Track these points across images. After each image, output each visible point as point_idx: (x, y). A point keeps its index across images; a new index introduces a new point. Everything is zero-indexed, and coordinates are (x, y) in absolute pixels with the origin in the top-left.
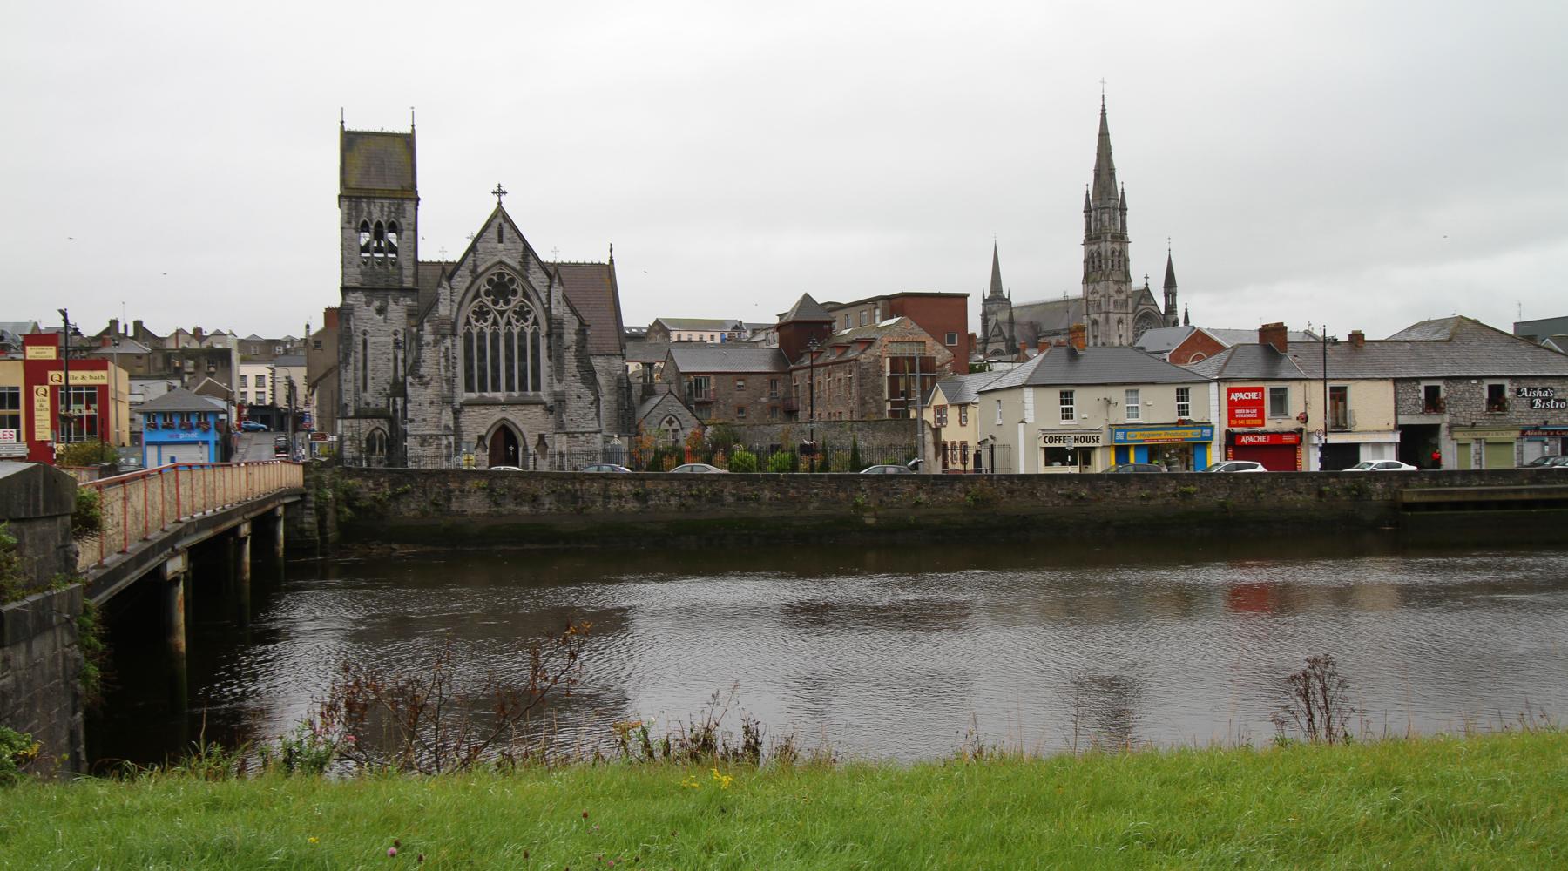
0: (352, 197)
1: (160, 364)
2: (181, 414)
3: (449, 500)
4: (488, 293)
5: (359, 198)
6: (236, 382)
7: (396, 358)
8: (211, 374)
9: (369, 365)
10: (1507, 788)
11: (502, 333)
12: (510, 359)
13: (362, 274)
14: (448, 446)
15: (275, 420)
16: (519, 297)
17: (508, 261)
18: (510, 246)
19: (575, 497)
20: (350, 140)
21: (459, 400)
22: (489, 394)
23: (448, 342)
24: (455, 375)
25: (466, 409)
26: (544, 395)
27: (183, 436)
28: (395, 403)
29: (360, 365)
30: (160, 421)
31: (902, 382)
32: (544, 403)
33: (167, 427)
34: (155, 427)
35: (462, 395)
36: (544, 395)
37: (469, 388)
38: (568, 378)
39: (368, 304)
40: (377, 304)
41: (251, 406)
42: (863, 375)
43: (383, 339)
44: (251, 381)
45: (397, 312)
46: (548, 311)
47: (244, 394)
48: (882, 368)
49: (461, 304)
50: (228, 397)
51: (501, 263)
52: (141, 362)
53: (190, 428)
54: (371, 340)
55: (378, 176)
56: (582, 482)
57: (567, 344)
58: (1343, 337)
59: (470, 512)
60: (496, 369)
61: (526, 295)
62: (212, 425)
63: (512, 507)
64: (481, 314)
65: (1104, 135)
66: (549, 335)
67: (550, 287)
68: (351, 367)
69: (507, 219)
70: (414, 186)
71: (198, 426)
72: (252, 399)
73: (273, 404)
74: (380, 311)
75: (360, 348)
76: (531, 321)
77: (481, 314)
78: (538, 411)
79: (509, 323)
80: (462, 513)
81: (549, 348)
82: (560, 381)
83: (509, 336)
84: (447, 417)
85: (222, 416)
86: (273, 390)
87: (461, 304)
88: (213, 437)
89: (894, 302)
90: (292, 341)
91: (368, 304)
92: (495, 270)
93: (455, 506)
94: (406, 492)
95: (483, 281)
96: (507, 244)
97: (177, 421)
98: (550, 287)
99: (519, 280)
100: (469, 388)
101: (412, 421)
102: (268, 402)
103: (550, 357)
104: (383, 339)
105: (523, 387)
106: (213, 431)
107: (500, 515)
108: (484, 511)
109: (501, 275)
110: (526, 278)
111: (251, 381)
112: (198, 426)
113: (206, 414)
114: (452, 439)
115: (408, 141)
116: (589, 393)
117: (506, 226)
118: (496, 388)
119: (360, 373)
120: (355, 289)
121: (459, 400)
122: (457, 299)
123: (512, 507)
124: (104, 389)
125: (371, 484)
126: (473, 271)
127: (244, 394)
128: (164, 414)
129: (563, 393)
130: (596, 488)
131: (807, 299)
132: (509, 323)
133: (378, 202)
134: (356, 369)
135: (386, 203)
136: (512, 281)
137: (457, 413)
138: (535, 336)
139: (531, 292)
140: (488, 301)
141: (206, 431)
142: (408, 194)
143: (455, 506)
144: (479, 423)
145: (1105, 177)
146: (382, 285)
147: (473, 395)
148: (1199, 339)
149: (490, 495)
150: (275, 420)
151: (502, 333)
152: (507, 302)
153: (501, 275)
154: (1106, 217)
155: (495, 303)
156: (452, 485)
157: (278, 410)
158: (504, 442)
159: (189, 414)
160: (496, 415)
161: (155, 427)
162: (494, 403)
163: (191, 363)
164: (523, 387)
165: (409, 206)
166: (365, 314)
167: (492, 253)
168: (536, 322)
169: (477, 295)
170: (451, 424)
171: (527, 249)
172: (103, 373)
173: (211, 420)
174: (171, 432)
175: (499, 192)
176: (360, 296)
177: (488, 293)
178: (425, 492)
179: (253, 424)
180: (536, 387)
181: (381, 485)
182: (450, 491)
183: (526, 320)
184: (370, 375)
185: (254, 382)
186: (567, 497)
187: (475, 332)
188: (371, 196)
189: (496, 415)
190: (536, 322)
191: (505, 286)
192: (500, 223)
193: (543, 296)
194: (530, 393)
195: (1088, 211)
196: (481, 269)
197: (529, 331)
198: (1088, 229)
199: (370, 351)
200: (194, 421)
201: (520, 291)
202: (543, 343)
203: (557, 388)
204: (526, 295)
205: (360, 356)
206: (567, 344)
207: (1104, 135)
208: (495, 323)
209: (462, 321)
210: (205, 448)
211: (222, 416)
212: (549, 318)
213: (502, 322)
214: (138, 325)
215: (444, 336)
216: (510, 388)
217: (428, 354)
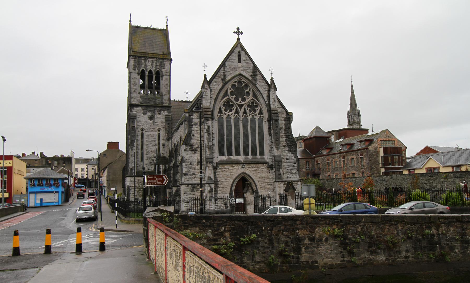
0: (136, 56)
1: (44, 163)
2: (46, 179)
3: (298, 250)
4: (232, 93)
5: (141, 57)
6: (73, 170)
8: (64, 167)
9: (145, 147)
11: (241, 118)
13: (141, 97)
14: (211, 191)
15: (88, 184)
16: (251, 97)
17: (245, 74)
18: (245, 65)
19: (432, 244)
20: (135, 31)
21: (216, 161)
22: (234, 157)
23: (210, 123)
24: (213, 145)
25: (220, 167)
26: (267, 157)
27: (47, 189)
28: (159, 168)
29: (140, 147)
30: (36, 183)
31: (390, 159)
32: (267, 163)
33: (40, 185)
34: (34, 185)
35: (218, 158)
36: (267, 157)
37: (221, 153)
38: (281, 147)
39: (144, 114)
40: (149, 114)
41: (79, 179)
42: (370, 156)
43: (152, 133)
44: (79, 170)
45: (160, 119)
46: (269, 105)
47: (76, 174)
48: (378, 153)
49: (216, 99)
50: (70, 174)
51: (240, 75)
52: (37, 162)
53: (50, 186)
54: (145, 134)
55: (149, 54)
56: (438, 227)
57: (281, 126)
59: (321, 262)
61: (255, 95)
62: (61, 184)
63: (366, 255)
64: (228, 106)
65: (352, 93)
66: (269, 120)
67: (269, 91)
68: (135, 148)
69: (243, 48)
70: (169, 53)
71: (54, 184)
72: (79, 176)
73: (87, 178)
74: (151, 118)
75: (140, 138)
76: (258, 112)
78: (264, 168)
79: (245, 112)
80: (313, 265)
81: (269, 128)
82: (278, 149)
84: (209, 172)
85: (66, 181)
86: (87, 173)
87: (216, 99)
88: (61, 189)
89: (340, 132)
90: (94, 159)
91: (144, 114)
92: (236, 79)
93: (304, 257)
94: (252, 242)
95: (229, 86)
96: (243, 63)
97: (44, 182)
98: (269, 91)
99: (251, 86)
100: (221, 153)
101: (186, 174)
102: (85, 177)
103: (270, 134)
104: (152, 133)
105: (254, 153)
106: (61, 187)
107: (356, 266)
108: (336, 261)
109: (240, 82)
110: (255, 85)
111: (79, 170)
112: (54, 184)
113: (58, 179)
114: (213, 186)
115: (165, 33)
116: (293, 156)
117: (243, 53)
118: (238, 153)
119: (140, 152)
120: (137, 106)
121: (216, 161)
122: (214, 96)
123: (366, 255)
124: (10, 169)
125: (209, 233)
126: (223, 79)
127: (76, 174)
128: (38, 180)
129: (280, 157)
130: (452, 231)
131: (317, 128)
133: (150, 60)
134: (137, 149)
135: (155, 60)
136: (246, 86)
137: (215, 168)
138: (261, 120)
139: (258, 94)
140: (233, 98)
141: (58, 187)
142: (166, 57)
143: (304, 257)
144: (228, 176)
145: (354, 105)
146: (152, 103)
147: (224, 158)
148: (427, 150)
149: (344, 245)
150: (88, 184)
153: (240, 82)
154: (355, 118)
155: (237, 100)
156: (301, 233)
157: (89, 180)
158: (243, 185)
159: (50, 179)
160: (239, 170)
161: (34, 185)
162: (237, 163)
163: (56, 162)
164: (254, 153)
165: (166, 63)
166: (143, 118)
167: (235, 68)
168: (261, 113)
169: (226, 94)
170: (212, 176)
171: (255, 67)
172: (11, 161)
173: (60, 182)
174: (42, 188)
175: (238, 32)
176: (140, 110)
177: (232, 93)
178: (271, 241)
179: (80, 185)
180: (262, 153)
181: (222, 235)
182: (299, 240)
183: (255, 111)
184: (145, 152)
185: (80, 170)
186: (424, 243)
188: (146, 56)
189: (239, 170)
190: (261, 113)
191: (242, 90)
192: (238, 51)
193: (265, 96)
194: (258, 156)
195: (349, 116)
196: (228, 78)
198: (349, 122)
199: (145, 139)
200: (52, 182)
201: (251, 93)
202: (265, 126)
203: (276, 153)
205: (140, 142)
206: (281, 126)
207: (352, 93)
208: (237, 112)
209: (217, 110)
210: (57, 194)
211: (66, 181)
212: (270, 110)
213: (241, 112)
214: (42, 154)
215: (207, 119)
216: (246, 153)
217: (195, 130)
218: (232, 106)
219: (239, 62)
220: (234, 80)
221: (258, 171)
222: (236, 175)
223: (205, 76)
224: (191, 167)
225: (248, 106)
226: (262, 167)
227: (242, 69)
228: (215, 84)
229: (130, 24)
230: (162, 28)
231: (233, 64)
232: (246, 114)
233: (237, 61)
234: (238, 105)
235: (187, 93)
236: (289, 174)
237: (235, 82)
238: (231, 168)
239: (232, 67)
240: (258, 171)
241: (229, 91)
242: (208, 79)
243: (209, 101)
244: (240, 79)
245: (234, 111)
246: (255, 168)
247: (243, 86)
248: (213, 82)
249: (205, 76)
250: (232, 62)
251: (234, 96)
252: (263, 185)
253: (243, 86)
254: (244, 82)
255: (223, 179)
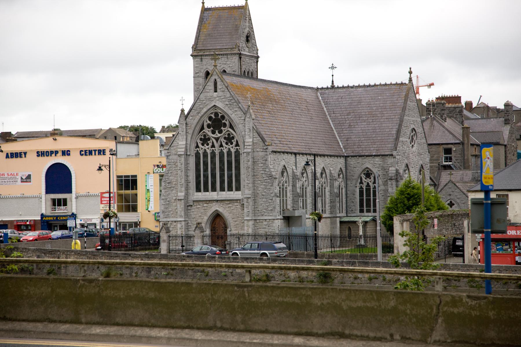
4: (209, 126)
7: (286, 197)
10: (227, 254)
12: (222, 170)
37: (198, 190)
55: (224, 41)
58: (502, 107)
60: (214, 176)
76: (234, 143)
77: (205, 140)
83: (221, 154)
100: (198, 190)
131: (508, 101)
132: (221, 146)
151: (217, 152)
152: (221, 132)
155: (221, 132)
167: (210, 99)
187: (201, 152)
197: (233, 150)
204: (231, 127)
218: (209, 139)
219: (216, 91)
220: (209, 112)
221: (232, 208)
222: (211, 213)
223: (183, 111)
225: (225, 138)
226: (236, 204)
228: (191, 118)
229: (203, 6)
230: (240, 5)
231: (208, 94)
232: (214, 147)
234: (215, 138)
235: (333, 68)
237: (212, 113)
238: (205, 205)
239: (208, 98)
240: (232, 208)
242: (186, 112)
243: (185, 136)
247: (219, 117)
249: (183, 111)
250: (208, 92)
251: (212, 128)
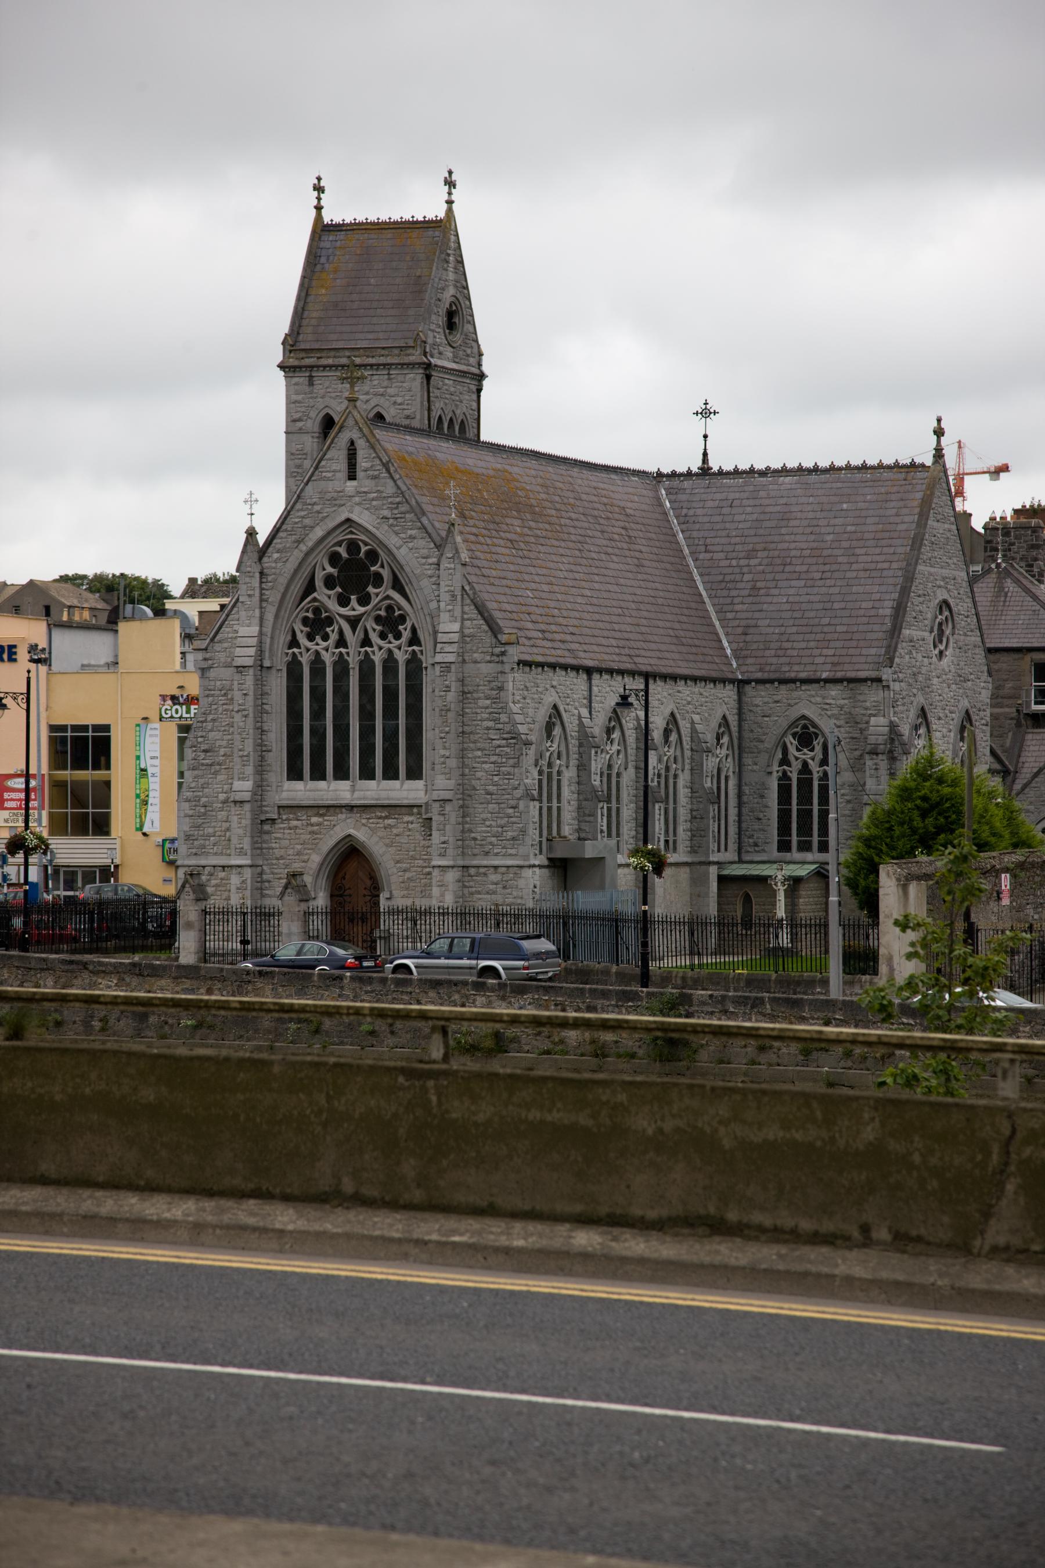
22: (118, 846)
76: (406, 635)
167: (337, 500)
218: (330, 621)
219: (352, 476)
220: (332, 540)
221: (395, 831)
224: (205, 814)
225: (378, 619)
226: (406, 818)
227: (357, 499)
228: (276, 556)
231: (331, 486)
232: (346, 646)
233: (343, 474)
234: (347, 619)
236: (491, 843)
237: (339, 544)
238: (314, 820)
239: (328, 496)
240: (395, 831)
241: (319, 576)
242: (261, 539)
244: (352, 533)
245: (334, 637)
246: (387, 822)
248: (271, 549)
249: (251, 533)
250: (329, 479)
251: (339, 589)
252: (408, 875)
253: (372, 569)
254: (366, 544)
255: (291, 852)
